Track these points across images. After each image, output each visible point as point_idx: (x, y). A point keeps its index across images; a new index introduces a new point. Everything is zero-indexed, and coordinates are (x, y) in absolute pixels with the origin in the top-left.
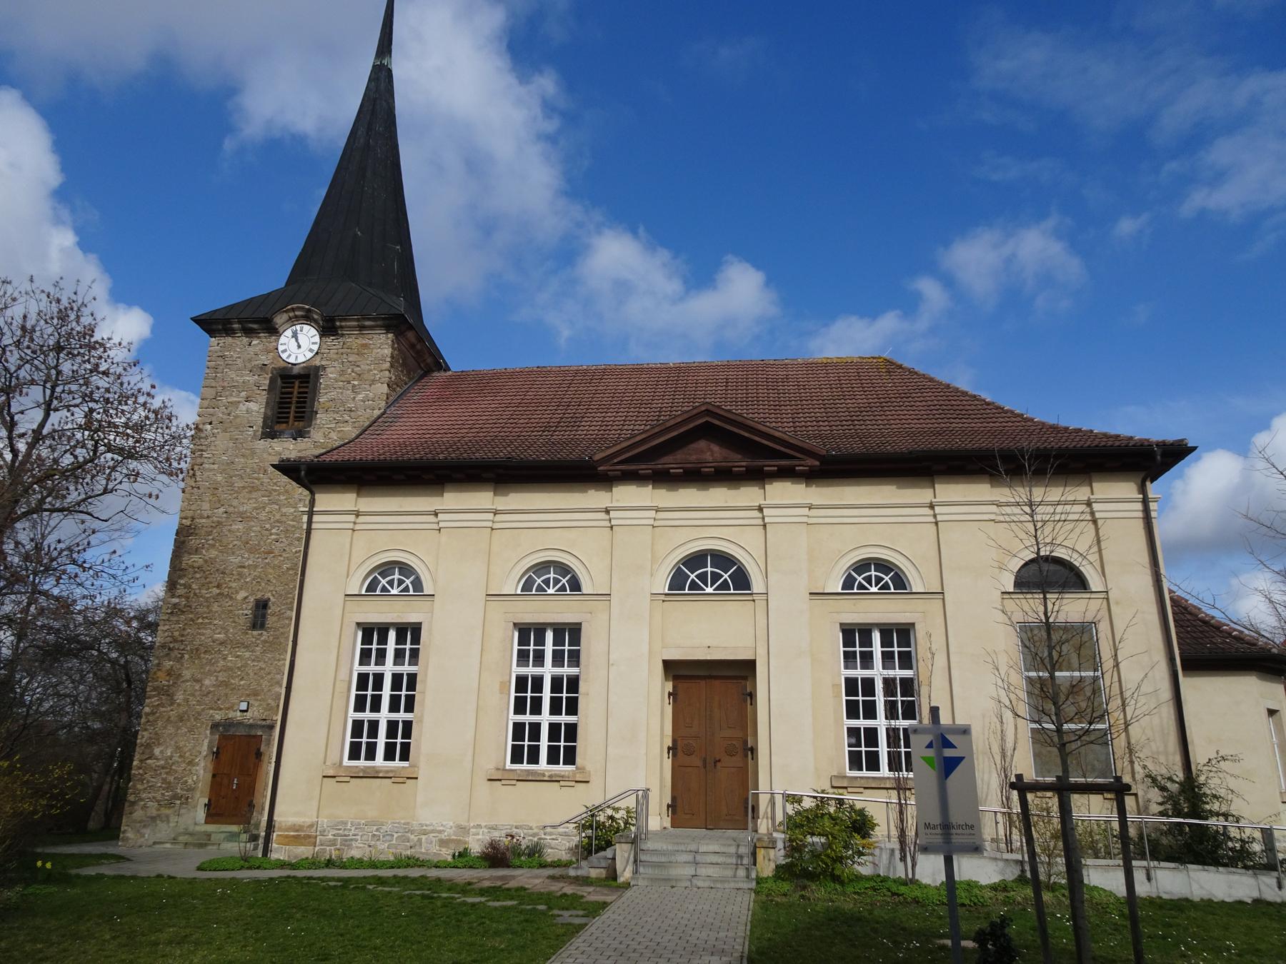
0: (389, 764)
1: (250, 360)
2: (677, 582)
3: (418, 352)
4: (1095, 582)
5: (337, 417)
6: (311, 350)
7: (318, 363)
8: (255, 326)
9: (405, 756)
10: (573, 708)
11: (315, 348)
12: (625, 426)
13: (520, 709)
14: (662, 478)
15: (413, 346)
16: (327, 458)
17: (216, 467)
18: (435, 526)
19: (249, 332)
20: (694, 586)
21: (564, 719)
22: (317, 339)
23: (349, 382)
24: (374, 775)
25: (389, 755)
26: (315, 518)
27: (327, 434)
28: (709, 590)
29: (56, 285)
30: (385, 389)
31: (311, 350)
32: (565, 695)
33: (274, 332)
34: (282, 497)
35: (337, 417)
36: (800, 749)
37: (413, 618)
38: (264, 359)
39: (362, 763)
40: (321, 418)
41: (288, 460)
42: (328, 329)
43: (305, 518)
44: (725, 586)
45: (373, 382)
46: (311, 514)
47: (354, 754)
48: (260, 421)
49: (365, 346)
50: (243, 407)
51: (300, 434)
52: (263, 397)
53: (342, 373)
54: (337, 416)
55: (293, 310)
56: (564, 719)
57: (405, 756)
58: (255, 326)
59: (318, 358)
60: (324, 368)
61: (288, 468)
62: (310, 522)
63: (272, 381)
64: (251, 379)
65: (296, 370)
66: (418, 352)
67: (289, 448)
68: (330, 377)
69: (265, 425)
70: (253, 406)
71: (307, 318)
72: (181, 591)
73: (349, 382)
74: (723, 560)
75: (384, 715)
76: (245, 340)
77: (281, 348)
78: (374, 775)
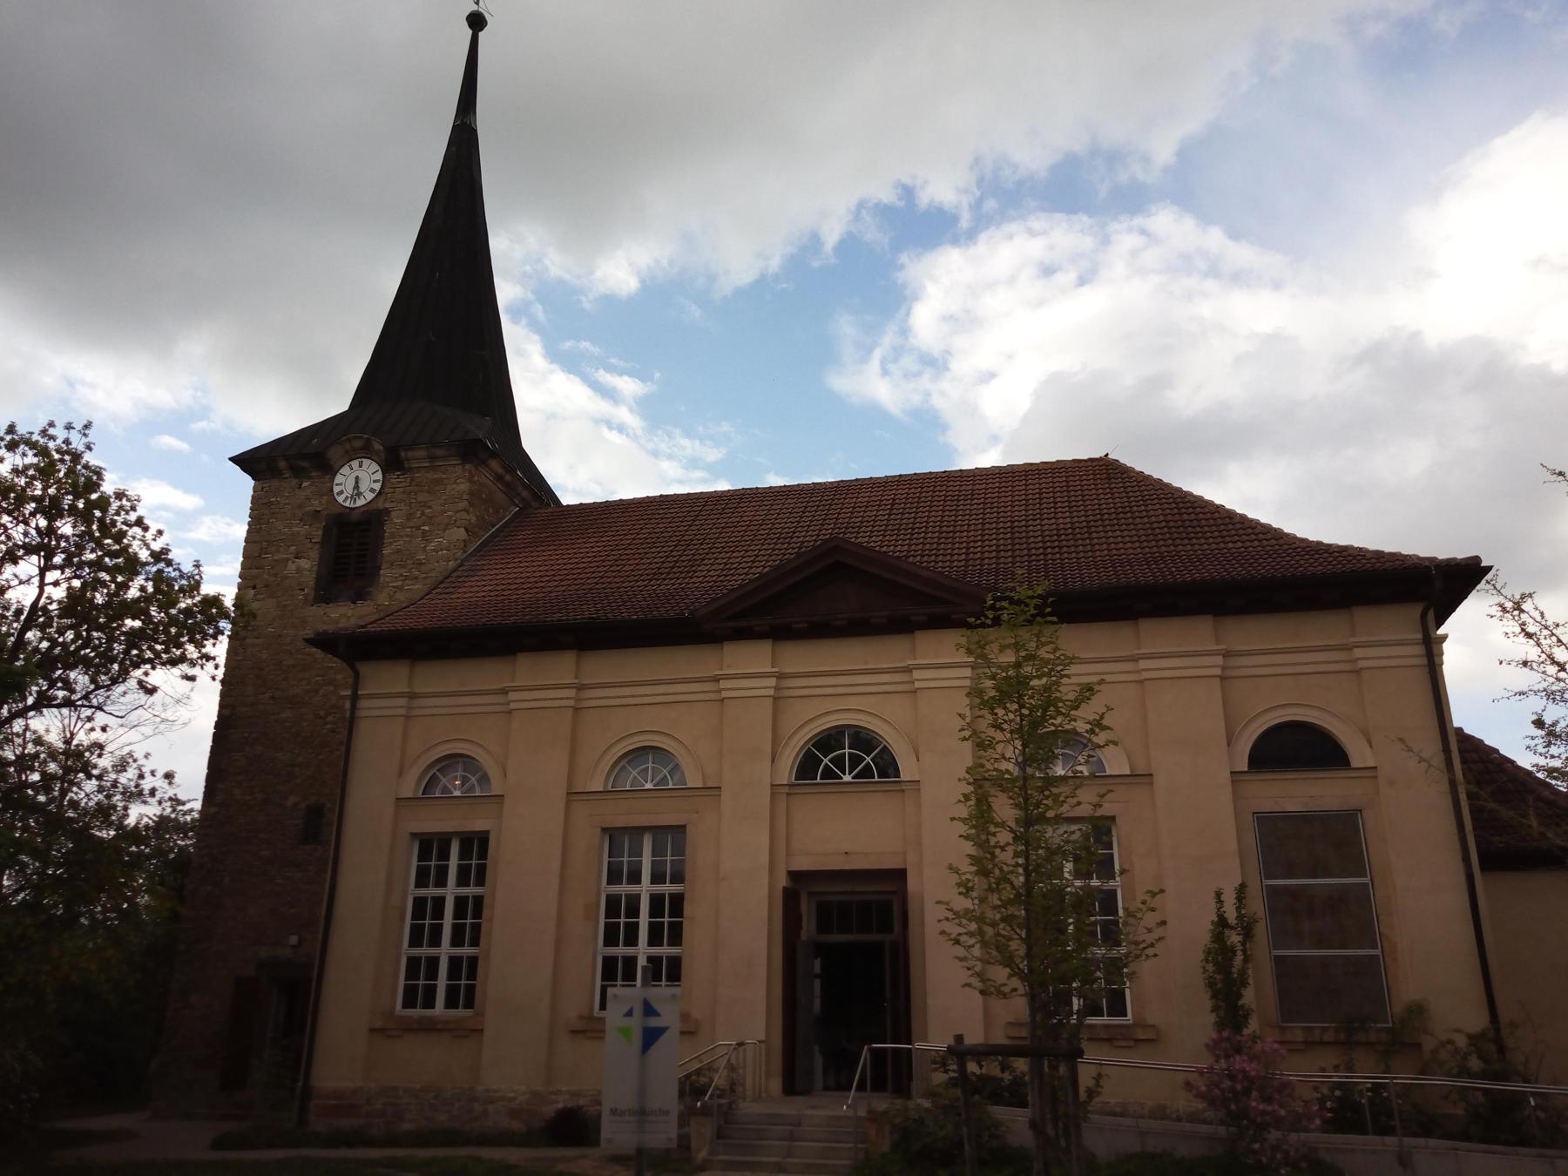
0: (410, 1012)
1: (300, 506)
2: (806, 767)
3: (507, 485)
4: (1360, 755)
5: (404, 572)
6: (372, 490)
7: (380, 505)
8: (305, 464)
9: (469, 1004)
10: (676, 937)
11: (377, 486)
12: (748, 564)
13: (611, 940)
14: (781, 634)
15: (499, 478)
16: (371, 628)
17: (260, 641)
18: (504, 708)
19: (299, 473)
20: (828, 774)
21: (665, 950)
22: (379, 476)
23: (418, 528)
24: (429, 1027)
25: (451, 1002)
26: (363, 703)
27: (396, 593)
28: (847, 778)
29: (44, 432)
30: (461, 534)
31: (372, 490)
32: (622, 920)
33: (331, 471)
34: (339, 676)
35: (404, 572)
36: (957, 998)
37: (478, 825)
38: (316, 504)
39: (417, 1012)
40: (386, 573)
41: (325, 633)
42: (391, 464)
43: (348, 705)
44: (866, 773)
45: (447, 527)
46: (355, 698)
47: (409, 1002)
48: (312, 583)
49: (439, 482)
50: (292, 566)
51: (359, 596)
52: (315, 554)
53: (410, 517)
54: (403, 571)
55: (349, 440)
56: (665, 950)
57: (469, 1004)
58: (305, 464)
59: (381, 500)
60: (387, 512)
61: (325, 642)
62: (354, 708)
63: (326, 531)
64: (302, 530)
65: (355, 517)
66: (507, 485)
67: (344, 616)
68: (397, 518)
69: (318, 587)
70: (304, 564)
71: (366, 452)
72: (1005, 726)
73: (418, 528)
74: (864, 740)
75: (445, 950)
76: (294, 482)
77: (336, 489)
78: (429, 1027)
